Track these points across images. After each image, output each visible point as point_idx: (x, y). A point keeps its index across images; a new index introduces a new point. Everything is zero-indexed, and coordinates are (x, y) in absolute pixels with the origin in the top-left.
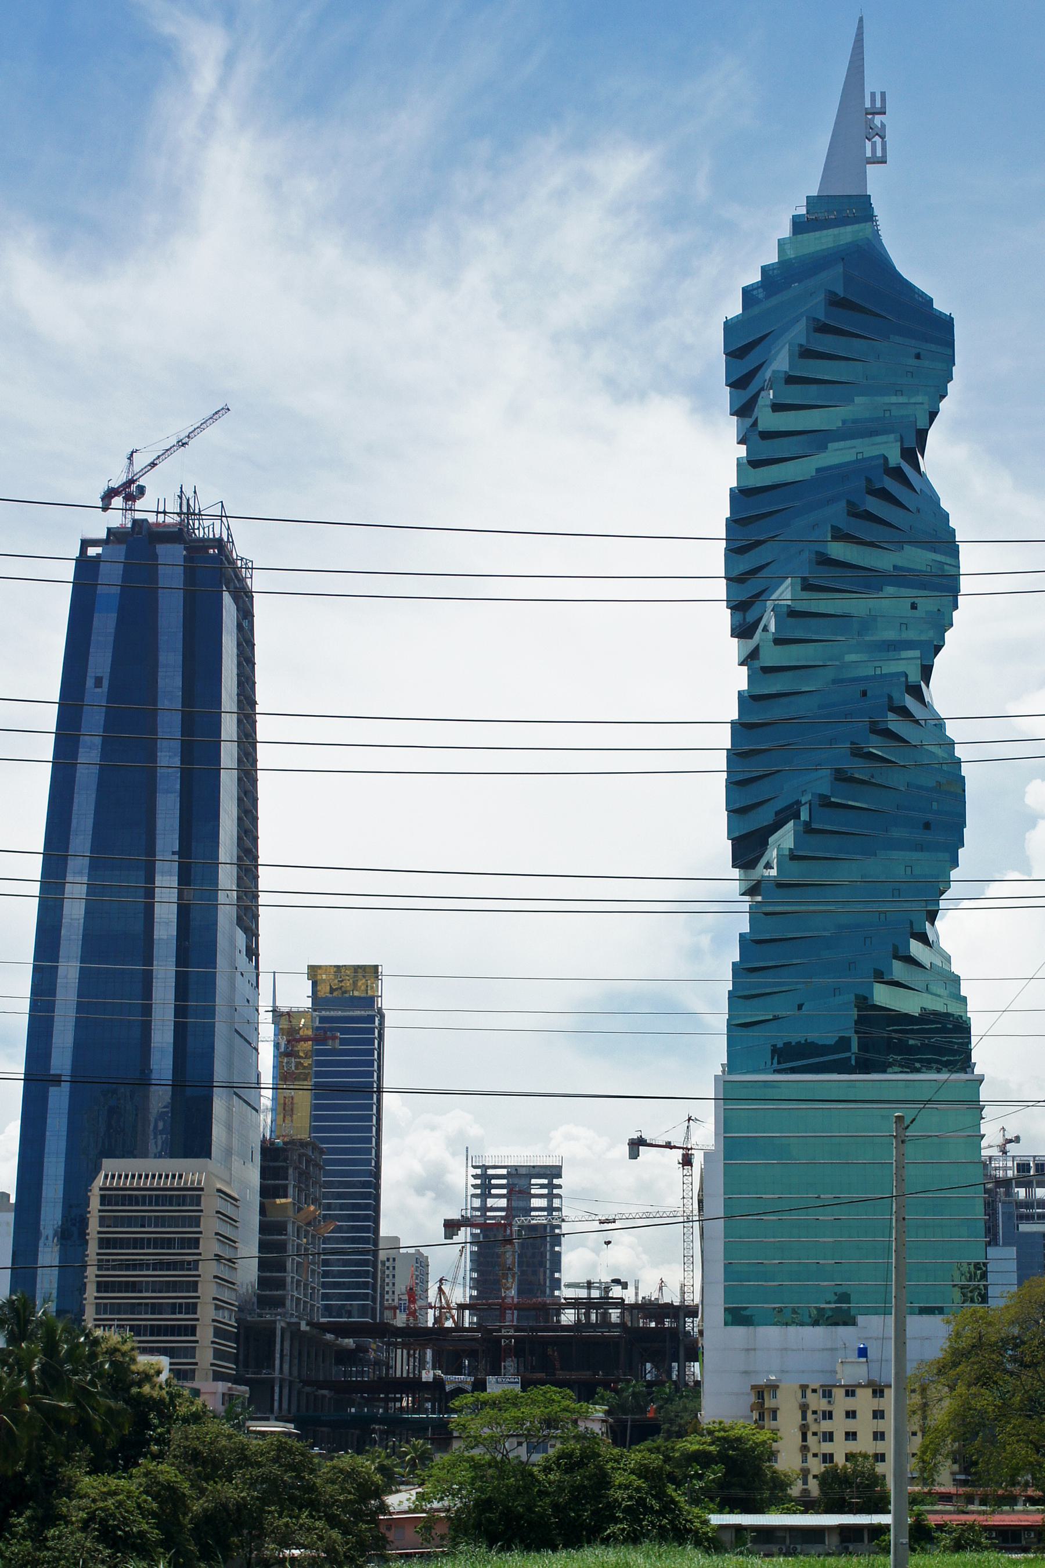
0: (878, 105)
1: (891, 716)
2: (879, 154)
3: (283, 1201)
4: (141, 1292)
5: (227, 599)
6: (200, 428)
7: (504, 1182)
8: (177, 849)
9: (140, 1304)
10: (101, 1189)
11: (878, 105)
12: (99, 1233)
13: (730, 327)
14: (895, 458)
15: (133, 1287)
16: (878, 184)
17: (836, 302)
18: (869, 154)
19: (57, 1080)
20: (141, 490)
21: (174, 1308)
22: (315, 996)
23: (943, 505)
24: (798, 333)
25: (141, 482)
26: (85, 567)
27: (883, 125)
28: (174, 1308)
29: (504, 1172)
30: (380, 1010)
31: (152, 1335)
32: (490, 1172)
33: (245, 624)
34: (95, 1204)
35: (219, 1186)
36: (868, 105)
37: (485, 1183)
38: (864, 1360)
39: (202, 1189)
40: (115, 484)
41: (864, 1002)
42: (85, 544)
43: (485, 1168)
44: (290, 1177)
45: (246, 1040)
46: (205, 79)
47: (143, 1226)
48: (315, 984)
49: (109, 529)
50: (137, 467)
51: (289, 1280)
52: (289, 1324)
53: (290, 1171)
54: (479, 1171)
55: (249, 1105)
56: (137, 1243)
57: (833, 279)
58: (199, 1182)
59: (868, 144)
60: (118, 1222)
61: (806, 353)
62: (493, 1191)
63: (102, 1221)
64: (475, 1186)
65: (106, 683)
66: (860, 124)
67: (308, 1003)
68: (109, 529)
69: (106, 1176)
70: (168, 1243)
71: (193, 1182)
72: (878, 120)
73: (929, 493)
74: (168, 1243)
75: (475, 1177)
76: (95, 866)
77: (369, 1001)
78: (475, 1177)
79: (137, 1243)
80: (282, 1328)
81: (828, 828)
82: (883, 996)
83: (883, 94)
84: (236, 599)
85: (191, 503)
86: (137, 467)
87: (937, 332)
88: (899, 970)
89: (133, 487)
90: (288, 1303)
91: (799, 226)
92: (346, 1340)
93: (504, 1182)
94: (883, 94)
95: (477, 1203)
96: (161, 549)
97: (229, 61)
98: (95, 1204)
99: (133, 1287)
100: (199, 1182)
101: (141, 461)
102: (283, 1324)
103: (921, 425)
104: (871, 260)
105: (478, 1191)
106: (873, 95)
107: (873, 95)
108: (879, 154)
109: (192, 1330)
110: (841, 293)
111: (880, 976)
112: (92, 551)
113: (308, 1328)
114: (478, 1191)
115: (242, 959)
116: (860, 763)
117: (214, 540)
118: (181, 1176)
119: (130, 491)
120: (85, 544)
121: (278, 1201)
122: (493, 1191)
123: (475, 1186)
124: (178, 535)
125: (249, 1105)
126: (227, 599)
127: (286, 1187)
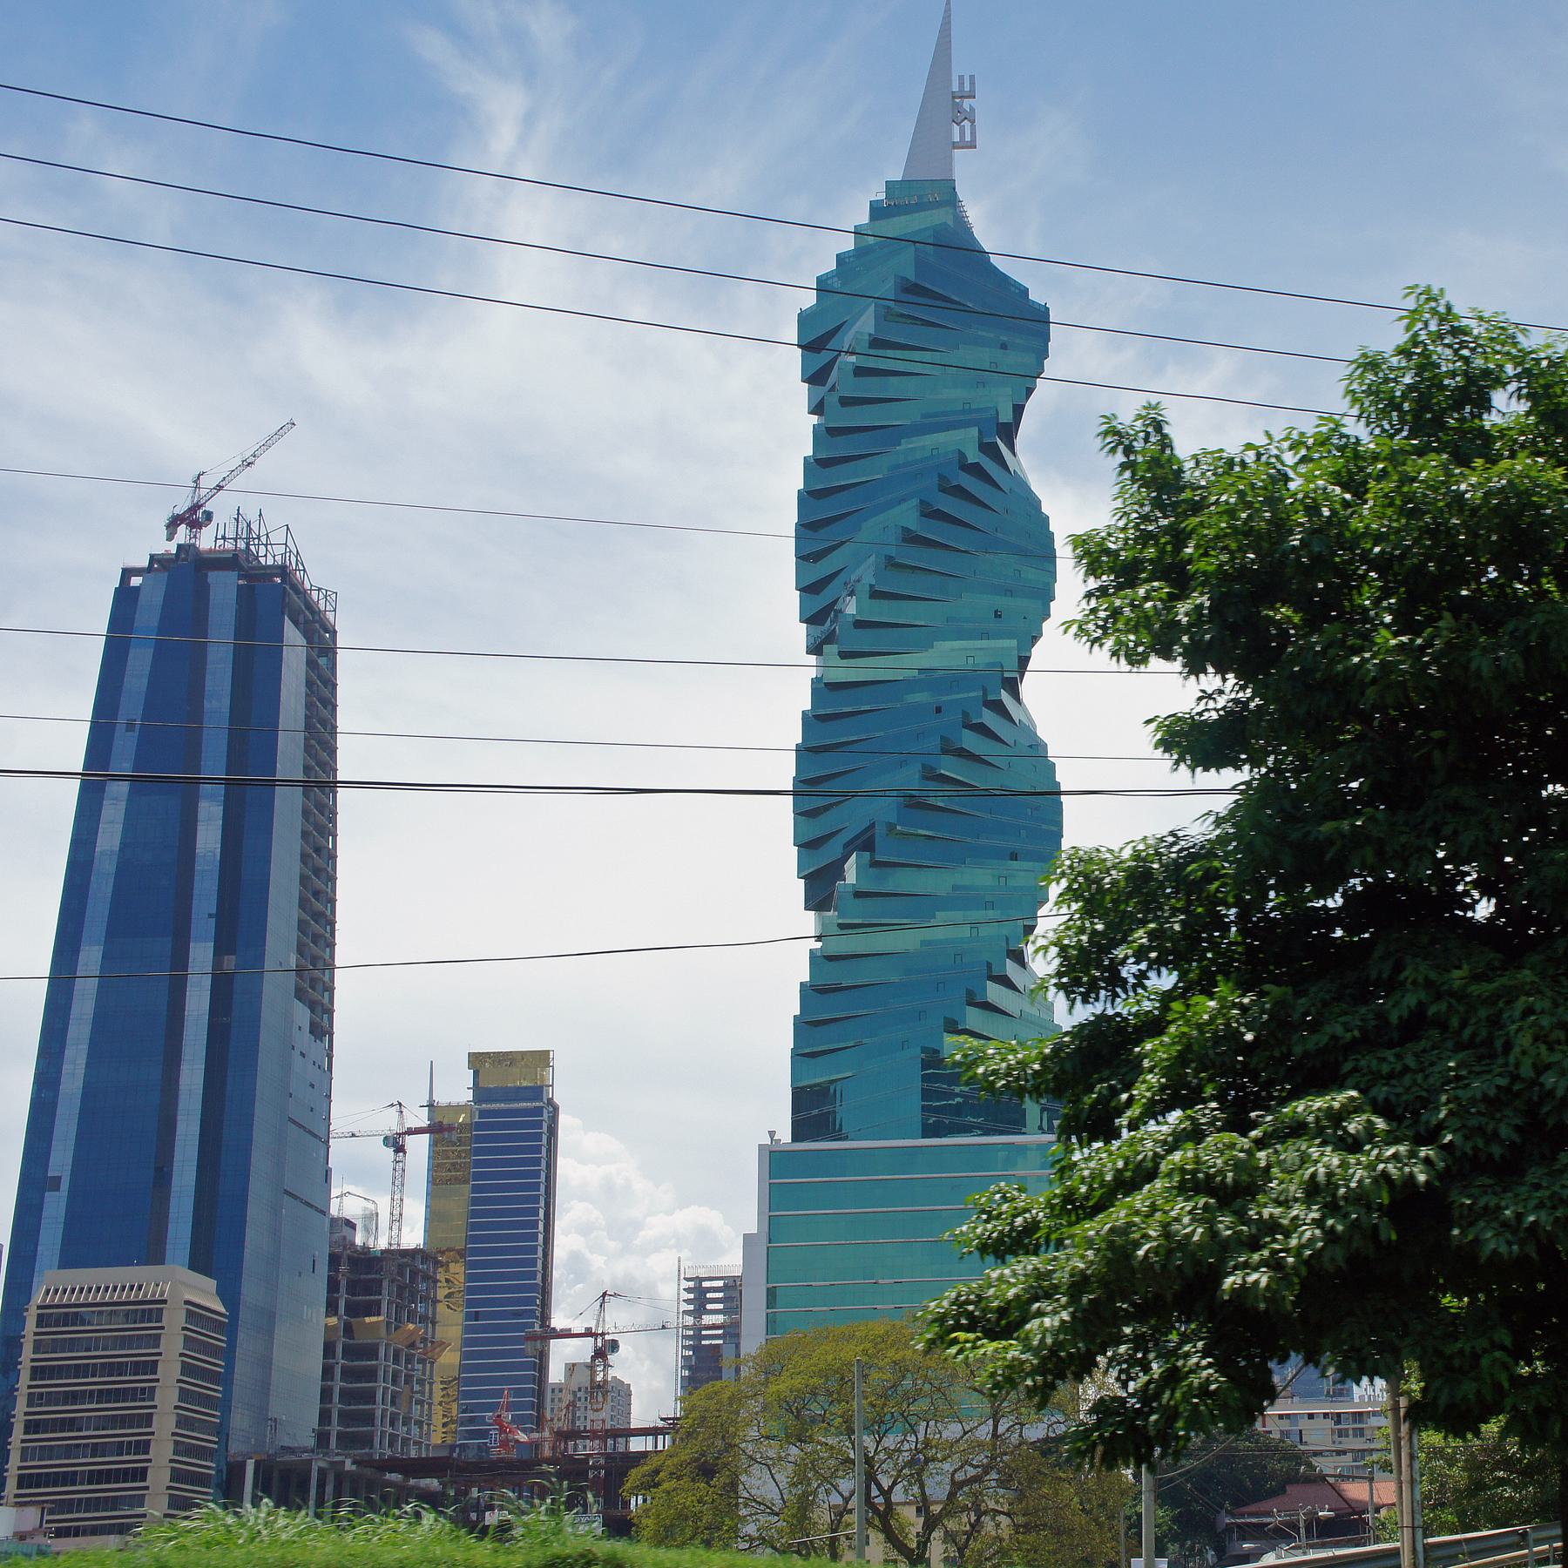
0: (967, 88)
1: (966, 733)
2: (968, 138)
3: (374, 1319)
4: (80, 1430)
5: (292, 634)
6: (266, 446)
7: (721, 1295)
8: (214, 911)
9: (78, 1446)
10: (39, 1307)
11: (967, 88)
12: (33, 1360)
13: (804, 319)
14: (974, 456)
15: (71, 1424)
16: (966, 172)
17: (911, 538)
18: (957, 139)
19: (55, 1183)
20: (209, 516)
21: (120, 1449)
22: (476, 1087)
23: (1042, 733)
24: (866, 573)
25: (208, 507)
26: (125, 598)
27: (972, 109)
28: (120, 1449)
29: (720, 1283)
30: (550, 1102)
31: (90, 1483)
32: (706, 1284)
33: (322, 661)
34: (31, 1325)
35: (188, 1297)
36: (955, 88)
37: (699, 1296)
38: (1006, 675)
39: (165, 1302)
40: (179, 511)
41: (932, 1059)
42: (127, 573)
43: (700, 1280)
44: (385, 1292)
45: (310, 1132)
46: (502, 142)
47: (88, 1350)
48: (476, 1074)
49: (152, 556)
50: (208, 482)
51: (379, 1413)
52: (332, 1463)
53: (385, 1284)
54: (691, 1284)
55: (311, 1206)
56: (79, 1371)
57: (905, 264)
58: (162, 1294)
59: (956, 128)
60: (56, 1346)
61: (875, 594)
62: (709, 1307)
63: (38, 1347)
64: (687, 1301)
65: (121, 721)
66: (948, 109)
67: (470, 1095)
68: (152, 556)
69: (48, 1292)
70: (119, 1369)
71: (154, 1294)
72: (967, 103)
73: (1024, 720)
74: (119, 1369)
75: (688, 1290)
76: (112, 933)
77: (538, 1092)
78: (688, 1290)
79: (79, 1371)
80: (320, 1470)
81: (896, 860)
82: (954, 1047)
83: (972, 78)
84: (308, 634)
85: (255, 527)
86: (203, 492)
87: (1030, 325)
88: (974, 1018)
89: (200, 513)
90: (377, 1440)
91: (877, 211)
92: (428, 1481)
93: (721, 1295)
94: (972, 78)
95: (690, 1320)
96: (213, 577)
97: (529, 121)
98: (31, 1325)
99: (71, 1424)
100: (162, 1294)
101: (208, 482)
102: (322, 1464)
103: (1006, 416)
104: (958, 248)
105: (691, 1307)
106: (961, 78)
107: (961, 78)
108: (968, 138)
109: (141, 1474)
110: (912, 278)
111: (953, 1028)
112: (136, 581)
113: (354, 1467)
114: (691, 1307)
115: (304, 1039)
116: (932, 785)
117: (278, 567)
118: (140, 1287)
119: (194, 518)
120: (127, 573)
121: (367, 1320)
122: (709, 1307)
123: (687, 1301)
124: (235, 562)
125: (311, 1206)
126: (292, 634)
127: (378, 1303)
